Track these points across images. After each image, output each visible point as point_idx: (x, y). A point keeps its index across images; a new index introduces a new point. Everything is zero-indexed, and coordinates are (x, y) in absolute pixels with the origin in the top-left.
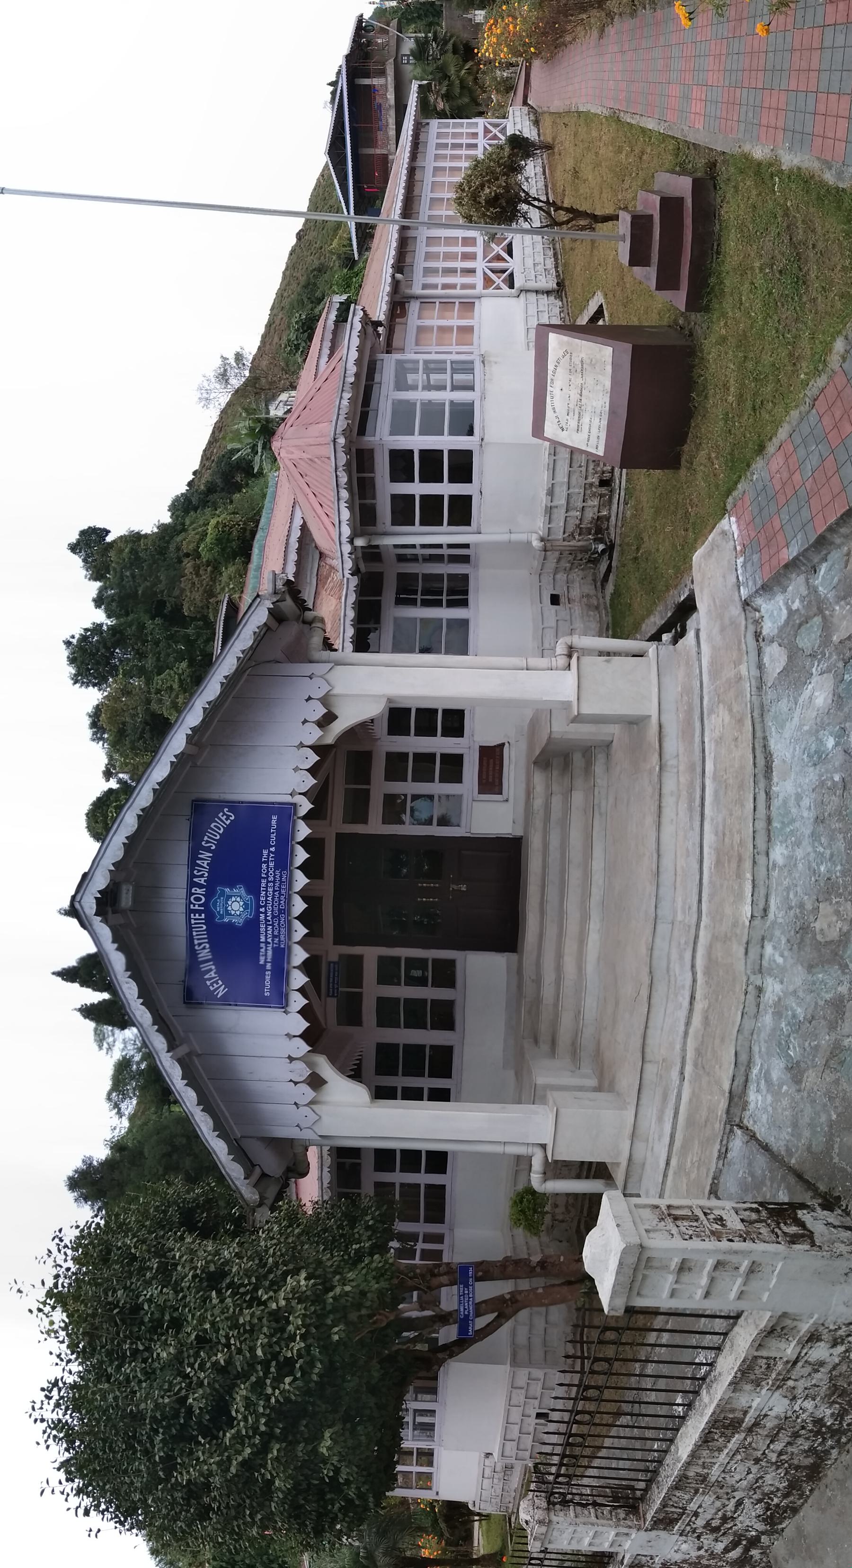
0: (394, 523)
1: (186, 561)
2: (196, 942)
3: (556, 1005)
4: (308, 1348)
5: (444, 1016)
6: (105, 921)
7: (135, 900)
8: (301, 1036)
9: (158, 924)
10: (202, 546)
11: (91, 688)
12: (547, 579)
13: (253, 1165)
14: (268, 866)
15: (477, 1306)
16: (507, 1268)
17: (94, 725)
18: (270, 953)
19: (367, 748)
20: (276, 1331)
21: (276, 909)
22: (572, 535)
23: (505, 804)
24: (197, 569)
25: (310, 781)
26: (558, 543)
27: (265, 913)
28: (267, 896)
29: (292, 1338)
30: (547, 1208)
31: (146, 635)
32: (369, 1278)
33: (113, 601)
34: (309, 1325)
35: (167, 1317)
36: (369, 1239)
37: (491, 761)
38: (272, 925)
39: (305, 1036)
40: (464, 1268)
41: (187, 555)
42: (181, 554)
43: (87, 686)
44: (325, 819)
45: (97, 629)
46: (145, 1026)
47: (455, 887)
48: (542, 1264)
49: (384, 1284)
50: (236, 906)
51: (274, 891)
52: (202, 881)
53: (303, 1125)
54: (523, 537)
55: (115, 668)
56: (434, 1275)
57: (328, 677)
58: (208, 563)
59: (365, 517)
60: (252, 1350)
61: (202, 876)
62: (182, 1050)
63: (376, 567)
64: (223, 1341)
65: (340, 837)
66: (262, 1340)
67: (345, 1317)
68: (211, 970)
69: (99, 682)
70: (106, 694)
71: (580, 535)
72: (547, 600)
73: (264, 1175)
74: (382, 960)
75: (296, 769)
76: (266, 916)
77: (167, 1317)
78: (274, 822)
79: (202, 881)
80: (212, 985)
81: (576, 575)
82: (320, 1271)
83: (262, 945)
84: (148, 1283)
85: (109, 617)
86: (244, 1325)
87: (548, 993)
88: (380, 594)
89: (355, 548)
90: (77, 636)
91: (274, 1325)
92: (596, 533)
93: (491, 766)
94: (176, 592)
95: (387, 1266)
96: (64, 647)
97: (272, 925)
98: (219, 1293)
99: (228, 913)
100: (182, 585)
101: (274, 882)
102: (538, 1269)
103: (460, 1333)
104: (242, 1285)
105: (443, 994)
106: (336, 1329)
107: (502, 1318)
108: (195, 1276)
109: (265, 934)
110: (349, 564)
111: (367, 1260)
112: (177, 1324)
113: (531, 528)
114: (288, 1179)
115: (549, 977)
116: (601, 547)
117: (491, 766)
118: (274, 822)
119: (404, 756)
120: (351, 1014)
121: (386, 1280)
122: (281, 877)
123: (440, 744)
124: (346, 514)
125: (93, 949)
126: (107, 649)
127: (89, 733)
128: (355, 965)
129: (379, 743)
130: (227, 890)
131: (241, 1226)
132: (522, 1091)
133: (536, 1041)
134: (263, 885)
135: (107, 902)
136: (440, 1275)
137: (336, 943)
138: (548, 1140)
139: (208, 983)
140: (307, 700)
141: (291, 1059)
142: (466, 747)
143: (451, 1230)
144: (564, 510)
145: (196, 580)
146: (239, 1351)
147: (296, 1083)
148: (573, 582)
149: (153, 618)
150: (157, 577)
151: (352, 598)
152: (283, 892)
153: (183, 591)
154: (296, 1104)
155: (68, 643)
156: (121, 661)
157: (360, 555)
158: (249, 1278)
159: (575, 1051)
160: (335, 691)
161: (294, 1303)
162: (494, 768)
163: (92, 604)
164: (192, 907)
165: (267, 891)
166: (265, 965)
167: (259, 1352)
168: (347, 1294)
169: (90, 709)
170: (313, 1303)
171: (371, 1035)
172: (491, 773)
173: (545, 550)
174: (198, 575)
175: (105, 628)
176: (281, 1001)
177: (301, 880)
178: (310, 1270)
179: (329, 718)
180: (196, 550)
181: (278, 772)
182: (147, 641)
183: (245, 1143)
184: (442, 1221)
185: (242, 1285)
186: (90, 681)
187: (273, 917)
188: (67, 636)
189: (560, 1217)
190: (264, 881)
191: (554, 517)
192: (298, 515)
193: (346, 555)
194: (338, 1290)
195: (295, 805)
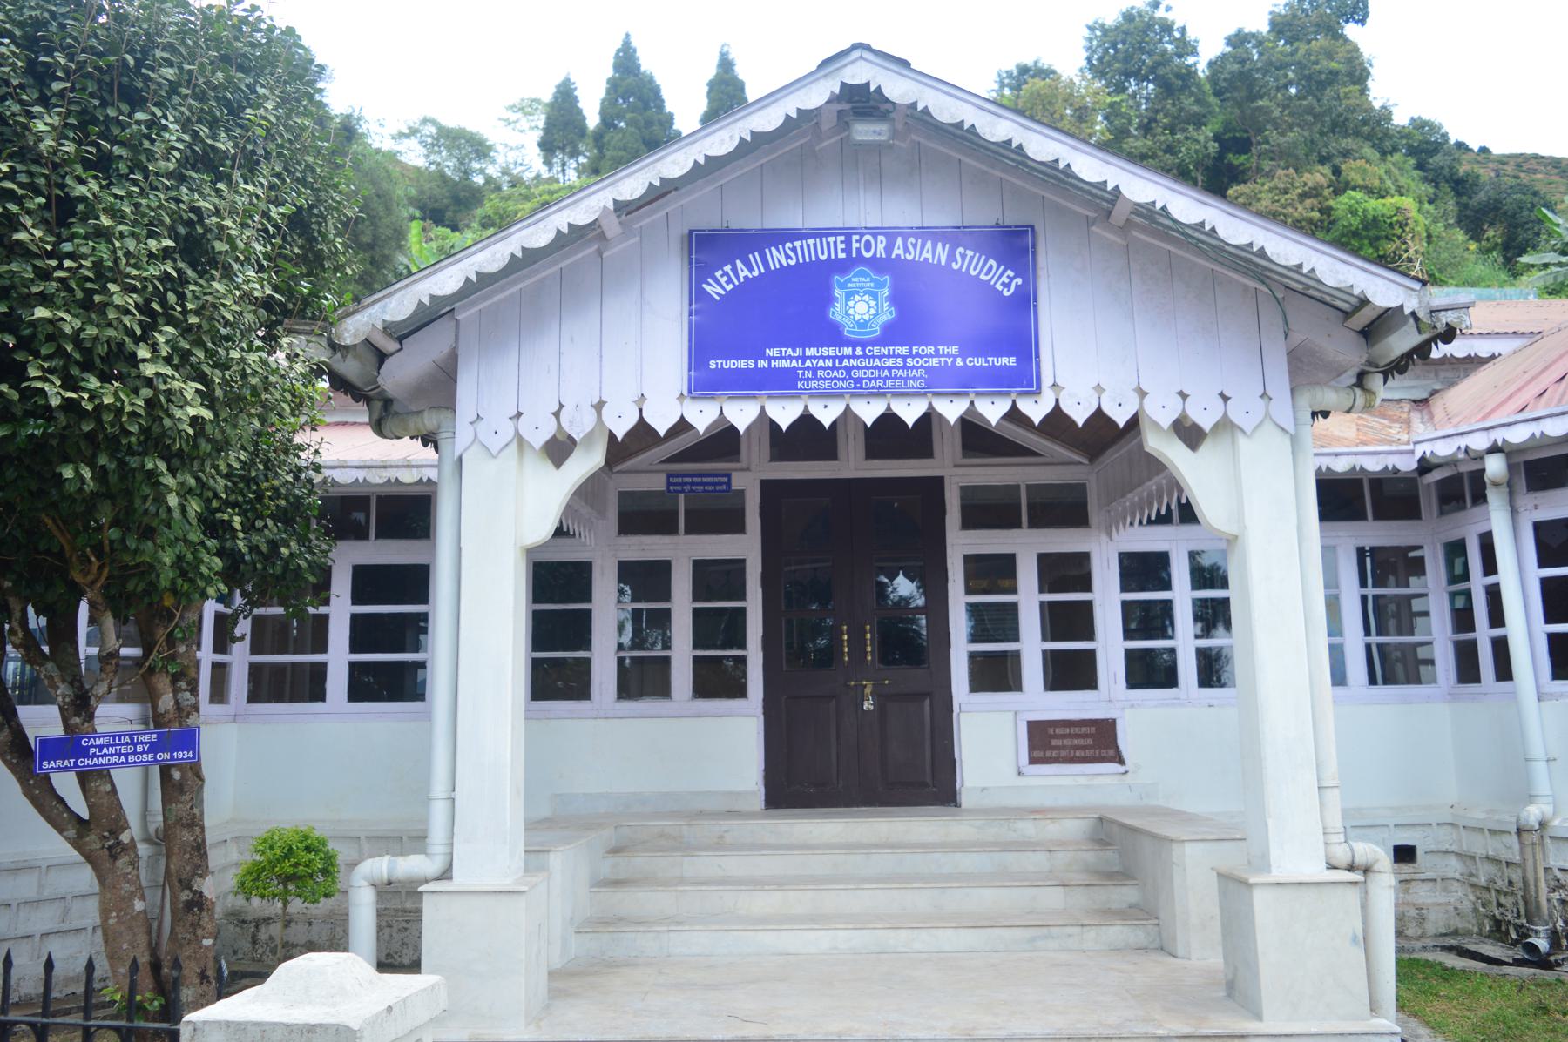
2: (797, 244)
4: (47, 412)
5: (643, 679)
8: (641, 419)
13: (400, 340)
14: (931, 356)
15: (103, 774)
16: (182, 835)
18: (785, 364)
19: (1094, 515)
20: (87, 353)
21: (861, 374)
27: (854, 356)
28: (880, 357)
29: (70, 383)
30: (296, 905)
32: (180, 547)
34: (99, 421)
35: (117, 150)
36: (253, 548)
39: (642, 430)
40: (189, 740)
44: (965, 456)
46: (659, 165)
48: (198, 903)
49: (166, 577)
51: (890, 369)
53: (481, 426)
56: (175, 679)
60: (45, 300)
62: (612, 227)
64: (67, 247)
65: (937, 483)
66: (70, 323)
67: (110, 496)
68: (751, 269)
73: (382, 357)
74: (739, 565)
75: (1099, 389)
76: (848, 357)
77: (117, 150)
80: (725, 274)
82: (205, 447)
83: (799, 352)
84: (185, 125)
86: (104, 291)
91: (102, 350)
95: (201, 583)
97: (834, 368)
98: (166, 254)
99: (849, 296)
101: (904, 367)
102: (185, 896)
103: (45, 742)
104: (181, 297)
106: (87, 473)
107: (78, 830)
108: (197, 210)
109: (819, 355)
110: (1444, 450)
111: (212, 543)
112: (102, 165)
114: (368, 400)
120: (640, 516)
121: (173, 581)
122: (914, 378)
130: (886, 292)
131: (282, 313)
132: (550, 823)
134: (898, 350)
136: (175, 692)
139: (728, 268)
141: (599, 406)
143: (235, 718)
146: (44, 275)
147: (557, 414)
152: (889, 383)
154: (519, 414)
158: (197, 313)
160: (1242, 441)
161: (146, 392)
164: (855, 237)
165: (889, 356)
166: (764, 358)
167: (41, 312)
168: (160, 500)
170: (144, 431)
171: (605, 553)
176: (704, 384)
178: (209, 429)
179: (1190, 434)
183: (444, 326)
185: (181, 297)
187: (848, 369)
189: (263, 936)
190: (904, 350)
193: (1463, 442)
194: (169, 480)
195: (1038, 392)
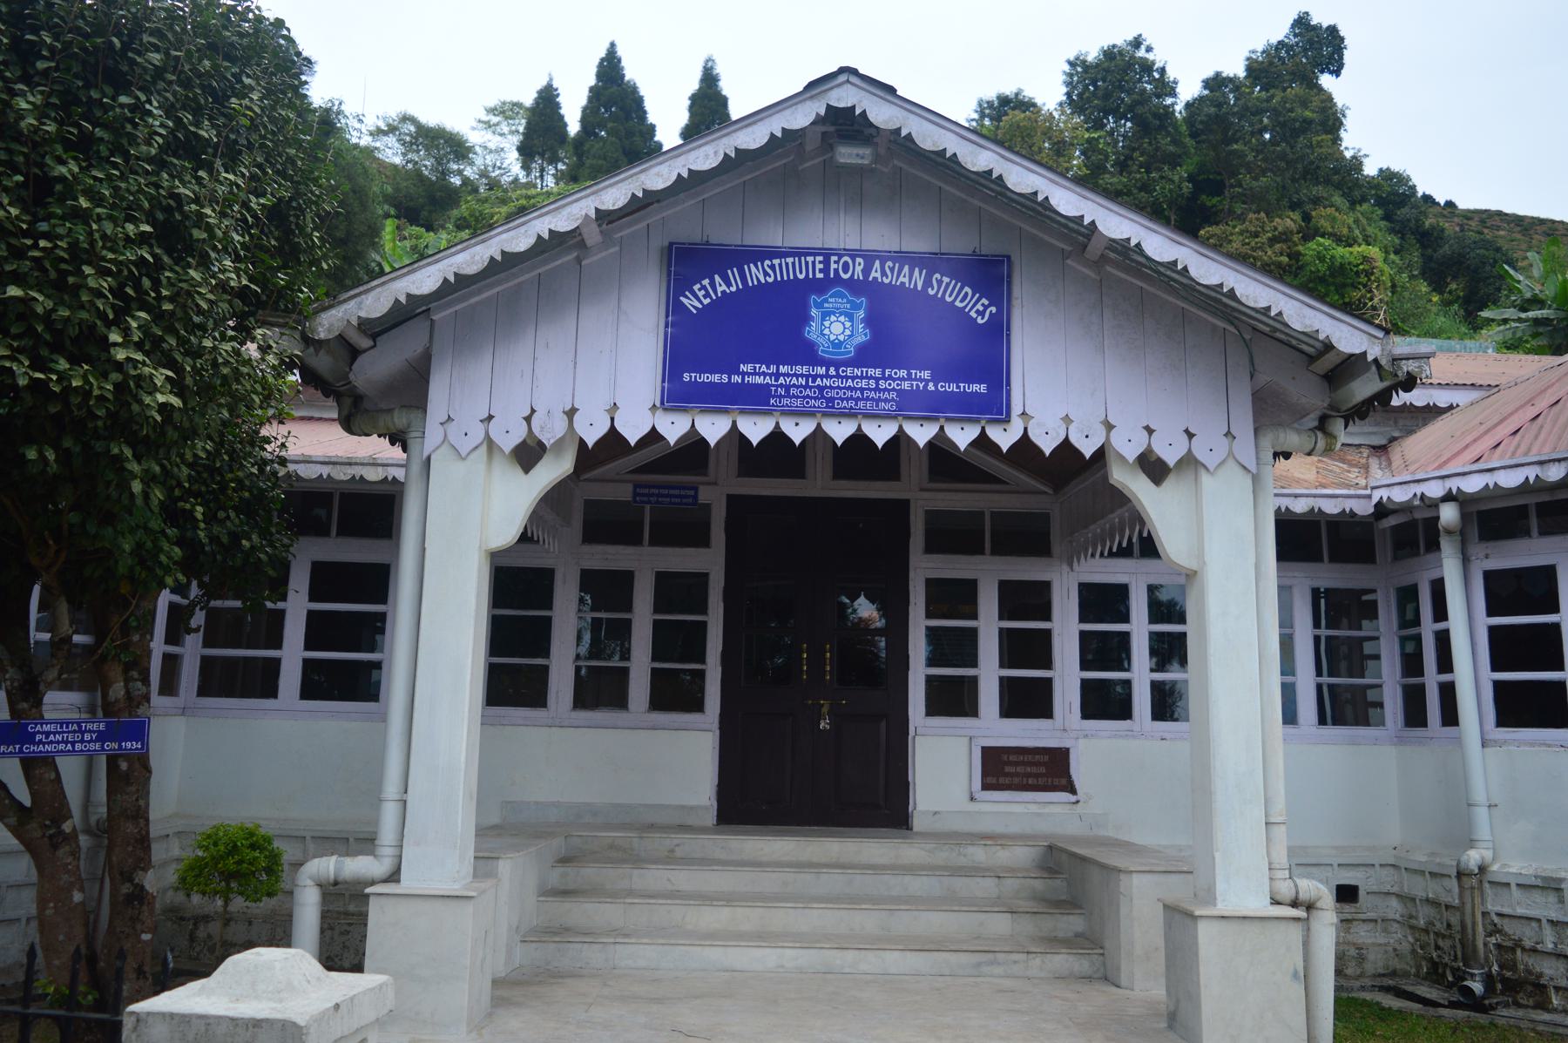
0: (1489, 576)
1: (1296, 216)
3: (631, 893)
5: (600, 690)
6: (818, 121)
7: (845, 166)
9: (743, 212)
10: (1327, 242)
11: (1064, 90)
12: (1387, 880)
14: (903, 379)
17: (1004, 101)
21: (833, 394)
22: (1495, 930)
23: (967, 797)
24: (1282, 237)
25: (1047, 446)
26: (1478, 900)
27: (827, 376)
31: (1160, 169)
33: (1219, 106)
37: (1043, 770)
38: (807, 386)
41: (1307, 218)
42: (1308, 207)
43: (1068, 84)
45: (1166, 87)
47: (825, 710)
50: (836, 328)
51: (862, 390)
52: (875, 274)
54: (1483, 830)
55: (1098, 125)
57: (1231, 463)
58: (1295, 256)
59: (1494, 518)
61: (884, 274)
63: (1383, 549)
69: (1077, 101)
70: (1056, 115)
71: (1499, 946)
72: (1348, 878)
74: (702, 579)
75: (1067, 420)
76: (822, 377)
78: (975, 388)
79: (875, 274)
81: (1400, 938)
85: (1188, 105)
87: (654, 877)
88: (1333, 559)
89: (1434, 504)
90: (1150, 56)
92: (1504, 980)
93: (1034, 770)
94: (1239, 208)
96: (1130, 38)
97: (807, 386)
99: (825, 315)
100: (1251, 216)
101: (877, 389)
105: (639, 687)
110: (1400, 496)
113: (1507, 848)
115: (682, 879)
116: (1477, 987)
117: (1034, 770)
118: (975, 388)
119: (1045, 613)
122: (886, 401)
123: (1067, 675)
124: (1509, 480)
125: (736, 112)
126: (1131, 108)
127: (991, 94)
128: (697, 536)
129: (1065, 567)
130: (861, 314)
132: (499, 830)
133: (564, 860)
134: (871, 372)
135: (844, 125)
137: (731, 499)
138: (408, 883)
140: (1187, 431)
142: (1065, 725)
143: (184, 711)
144: (1554, 916)
145: (1264, 238)
148: (1385, 930)
149: (1191, 179)
150: (1264, 172)
151: (1331, 508)
152: (861, 404)
153: (1241, 218)
155: (1137, 43)
156: (1111, 133)
157: (1418, 515)
159: (555, 934)
160: (1205, 478)
162: (1029, 775)
163: (1210, 73)
164: (834, 258)
165: (862, 378)
169: (1029, 93)
172: (1020, 769)
173: (1460, 875)
174: (1273, 241)
175: (1169, 101)
177: (922, 434)
179: (1154, 468)
180: (1318, 232)
181: (1062, 389)
182: (1148, 172)
184: (203, 691)
186: (1074, 88)
188: (1149, 40)
190: (877, 372)
191: (1537, 896)
192: (1460, 398)
193: (1419, 489)
195: (1007, 420)
